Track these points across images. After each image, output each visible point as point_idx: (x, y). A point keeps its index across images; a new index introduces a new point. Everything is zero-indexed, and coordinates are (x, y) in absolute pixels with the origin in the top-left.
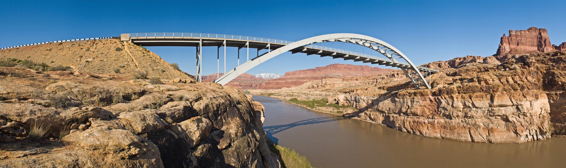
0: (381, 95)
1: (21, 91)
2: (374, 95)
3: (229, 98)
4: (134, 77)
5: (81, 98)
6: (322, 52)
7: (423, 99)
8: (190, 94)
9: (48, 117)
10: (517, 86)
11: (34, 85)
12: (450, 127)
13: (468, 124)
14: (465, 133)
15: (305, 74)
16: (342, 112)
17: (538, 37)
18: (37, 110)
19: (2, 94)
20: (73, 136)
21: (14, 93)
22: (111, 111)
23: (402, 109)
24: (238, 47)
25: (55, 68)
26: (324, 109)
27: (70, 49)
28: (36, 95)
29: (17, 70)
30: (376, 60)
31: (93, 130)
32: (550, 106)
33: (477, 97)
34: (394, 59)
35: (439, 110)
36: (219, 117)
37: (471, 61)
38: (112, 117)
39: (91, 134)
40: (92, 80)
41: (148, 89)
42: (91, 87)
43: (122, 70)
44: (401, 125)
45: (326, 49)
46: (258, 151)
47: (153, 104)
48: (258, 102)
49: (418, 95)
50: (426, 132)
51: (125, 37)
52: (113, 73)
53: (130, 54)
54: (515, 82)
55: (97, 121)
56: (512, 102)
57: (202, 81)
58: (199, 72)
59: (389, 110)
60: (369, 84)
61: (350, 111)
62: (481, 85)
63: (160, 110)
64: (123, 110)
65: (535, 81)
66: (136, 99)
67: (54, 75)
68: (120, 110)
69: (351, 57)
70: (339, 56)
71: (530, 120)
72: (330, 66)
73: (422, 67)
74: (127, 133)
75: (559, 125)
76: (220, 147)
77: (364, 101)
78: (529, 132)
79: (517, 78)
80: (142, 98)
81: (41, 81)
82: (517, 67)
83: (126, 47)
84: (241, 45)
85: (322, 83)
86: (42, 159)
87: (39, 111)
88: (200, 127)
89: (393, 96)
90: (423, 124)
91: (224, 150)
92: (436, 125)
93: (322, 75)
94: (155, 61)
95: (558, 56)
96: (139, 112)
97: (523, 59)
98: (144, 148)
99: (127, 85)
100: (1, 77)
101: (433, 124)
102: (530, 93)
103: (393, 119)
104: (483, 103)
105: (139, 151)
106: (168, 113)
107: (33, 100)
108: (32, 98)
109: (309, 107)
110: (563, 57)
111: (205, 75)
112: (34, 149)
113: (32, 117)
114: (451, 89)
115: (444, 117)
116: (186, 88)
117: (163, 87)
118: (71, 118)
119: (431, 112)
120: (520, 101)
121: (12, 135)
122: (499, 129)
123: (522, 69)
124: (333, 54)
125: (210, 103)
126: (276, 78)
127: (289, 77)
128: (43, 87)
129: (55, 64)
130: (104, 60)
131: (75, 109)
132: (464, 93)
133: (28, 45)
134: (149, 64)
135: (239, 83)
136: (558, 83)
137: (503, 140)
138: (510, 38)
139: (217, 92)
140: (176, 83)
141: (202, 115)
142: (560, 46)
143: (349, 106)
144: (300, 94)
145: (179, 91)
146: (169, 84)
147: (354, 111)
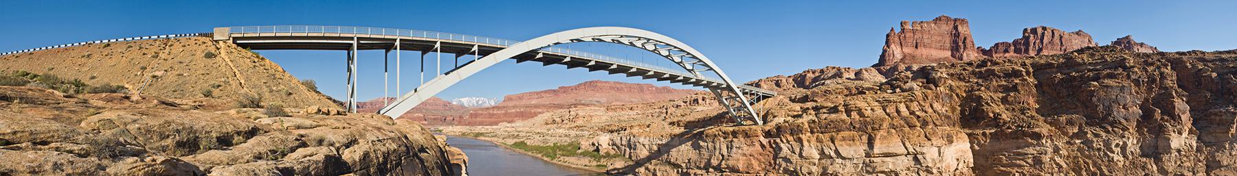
1: (38, 129)
10: (915, 120)
16: (606, 166)
17: (951, 34)
18: (65, 163)
19: (4, 134)
22: (197, 164)
23: (712, 161)
25: (97, 88)
29: (30, 92)
33: (844, 139)
35: (778, 162)
37: (834, 77)
42: (162, 121)
43: (216, 92)
45: (577, 55)
47: (270, 151)
48: (457, 149)
51: (221, 34)
52: (200, 97)
53: (230, 63)
54: (912, 113)
56: (906, 148)
59: (689, 162)
64: (218, 162)
65: (947, 111)
66: (241, 143)
67: (95, 101)
68: (213, 163)
69: (622, 69)
70: (599, 66)
73: (746, 87)
79: (915, 106)
80: (252, 141)
81: (73, 111)
82: (915, 86)
83: (222, 51)
84: (426, 47)
89: (695, 138)
95: (986, 66)
96: (246, 166)
99: (224, 118)
104: (855, 150)
107: (58, 144)
108: (57, 142)
109: (547, 157)
110: (996, 68)
114: (799, 126)
119: (763, 166)
125: (372, 150)
127: (510, 104)
130: (185, 74)
132: (822, 133)
133: (50, 48)
136: (988, 114)
139: (384, 130)
141: (357, 171)
142: (991, 50)
143: (618, 156)
144: (531, 134)
146: (299, 116)
147: (626, 165)
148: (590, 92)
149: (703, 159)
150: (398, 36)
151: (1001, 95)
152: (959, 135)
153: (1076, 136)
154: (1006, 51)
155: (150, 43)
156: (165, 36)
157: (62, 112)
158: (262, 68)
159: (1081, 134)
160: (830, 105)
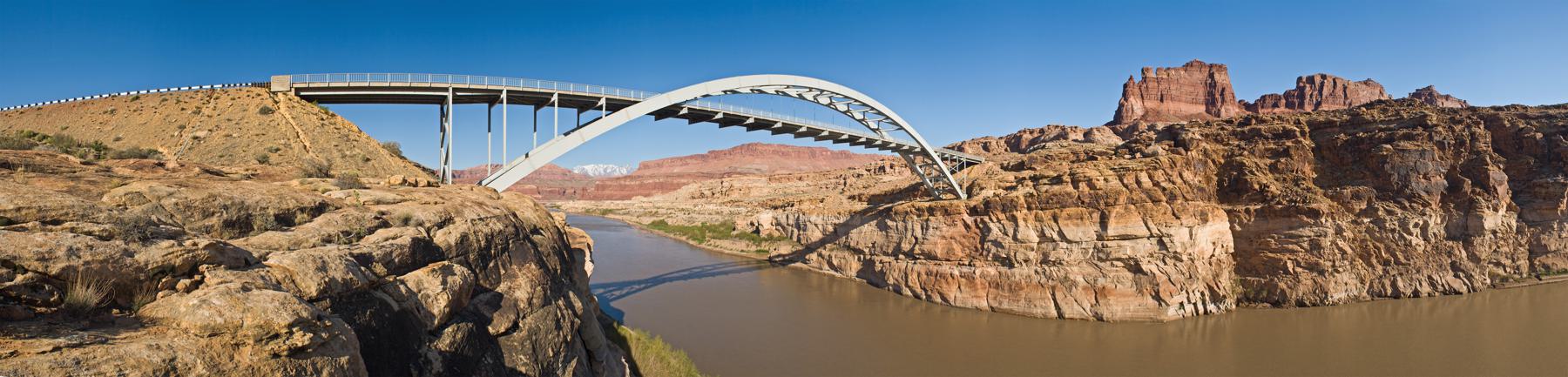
1: (48, 204)
2: (839, 214)
7: (949, 221)
9: (108, 263)
10: (1160, 193)
12: (1010, 286)
13: (1050, 278)
16: (767, 252)
18: (83, 248)
19: (5, 211)
20: (162, 306)
22: (250, 249)
23: (903, 245)
24: (533, 107)
25: (123, 152)
26: (727, 246)
29: (38, 158)
33: (1070, 217)
34: (884, 133)
35: (986, 247)
36: (490, 262)
37: (1057, 138)
38: (252, 263)
39: (205, 301)
41: (332, 200)
42: (205, 195)
43: (274, 158)
44: (900, 280)
45: (731, 110)
46: (578, 340)
47: (342, 232)
48: (580, 230)
49: (939, 213)
51: (280, 83)
52: (254, 164)
53: (291, 121)
54: (1156, 184)
56: (1148, 229)
57: (453, 183)
59: (874, 246)
61: (785, 249)
65: (1200, 182)
66: (306, 222)
67: (121, 169)
68: (269, 247)
70: (760, 125)
72: (741, 149)
73: (945, 151)
74: (285, 298)
76: (493, 329)
80: (319, 220)
81: (93, 181)
82: (1160, 150)
83: (282, 105)
84: (540, 101)
90: (950, 279)
91: (503, 338)
92: (978, 281)
96: (312, 252)
99: (285, 191)
101: (970, 279)
104: (1084, 231)
107: (74, 224)
109: (694, 239)
110: (1262, 127)
111: (460, 168)
113: (72, 264)
114: (1012, 200)
115: (997, 263)
119: (968, 251)
121: (25, 303)
123: (1172, 156)
124: (748, 122)
126: (621, 176)
127: (647, 173)
130: (234, 135)
132: (1042, 209)
133: (63, 101)
134: (334, 143)
136: (1252, 186)
139: (487, 206)
142: (1256, 104)
143: (784, 239)
144: (673, 211)
146: (379, 189)
147: (794, 250)
148: (748, 158)
150: (504, 86)
151: (1268, 161)
153: (1363, 213)
154: (1275, 105)
155: (191, 94)
158: (332, 127)
159: (1370, 211)
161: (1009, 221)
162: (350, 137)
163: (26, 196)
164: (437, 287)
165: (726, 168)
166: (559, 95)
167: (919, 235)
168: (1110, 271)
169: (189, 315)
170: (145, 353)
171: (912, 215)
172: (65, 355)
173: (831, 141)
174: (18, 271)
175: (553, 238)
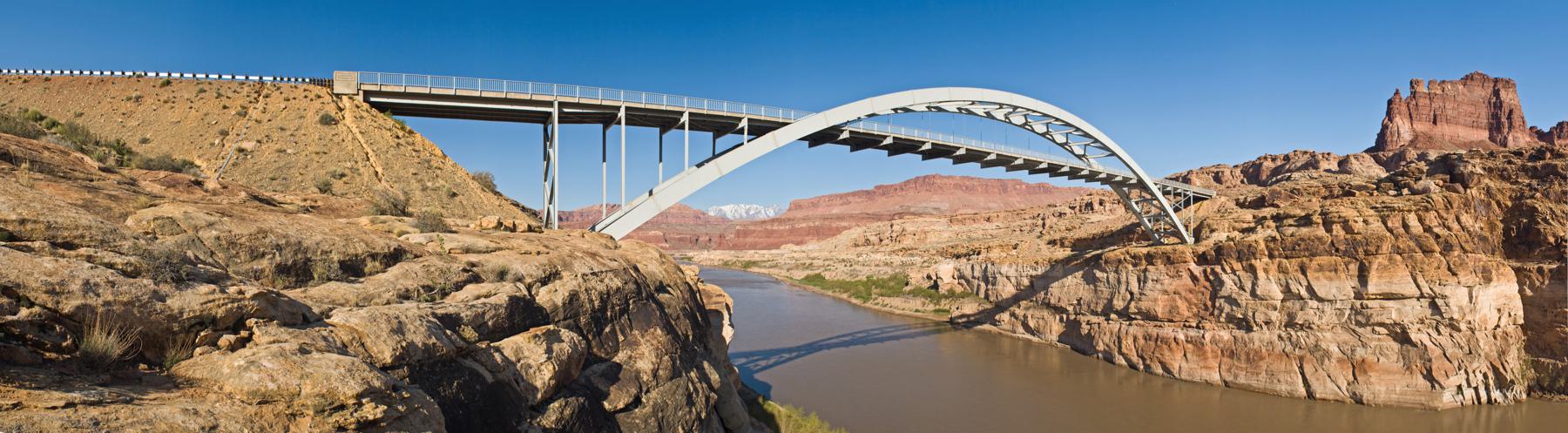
0: (1055, 261)
1: (60, 220)
2: (1037, 263)
3: (634, 275)
4: (372, 208)
5: (223, 262)
6: (892, 142)
7: (1172, 272)
8: (526, 263)
9: (134, 306)
10: (1432, 241)
11: (95, 206)
12: (1248, 354)
13: (1296, 345)
14: (1289, 372)
15: (846, 206)
16: (948, 311)
17: (1490, 103)
18: (102, 283)
19: (6, 221)
20: (200, 364)
21: (39, 222)
22: (309, 303)
23: (1115, 302)
24: (658, 129)
25: (151, 160)
26: (898, 304)
27: (193, 105)
28: (99, 238)
29: (46, 154)
30: (1041, 163)
31: (258, 353)
32: (1524, 305)
33: (1321, 268)
34: (1091, 160)
35: (1217, 304)
36: (606, 326)
37: (1305, 167)
38: (312, 320)
39: (253, 362)
40: (255, 210)
41: (410, 245)
42: (253, 229)
43: (338, 186)
44: (1112, 345)
45: (903, 133)
46: (714, 417)
47: (423, 287)
48: (716, 287)
49: (1159, 261)
50: (1180, 367)
51: (345, 82)
52: (313, 192)
53: (359, 136)
54: (1428, 229)
55: (270, 329)
56: (1418, 286)
57: (559, 227)
58: (551, 201)
59: (1079, 304)
60: (1021, 230)
61: (970, 308)
62: (1331, 235)
63: (443, 305)
64: (342, 301)
65: (1482, 229)
66: (378, 272)
67: (149, 184)
68: (333, 302)
69: (974, 156)
70: (939, 151)
71: (1469, 341)
72: (915, 183)
73: (1168, 183)
74: (353, 364)
75: (1548, 364)
76: (610, 404)
77: (1009, 280)
78: (1465, 376)
79: (1432, 218)
80: (395, 270)
81: (114, 196)
82: (1433, 187)
83: (347, 114)
84: (666, 122)
85: (892, 231)
86: (117, 419)
87: (109, 285)
88: (554, 354)
89: (1088, 265)
90: (1173, 345)
91: (623, 414)
92: (1208, 348)
93: (892, 209)
94: (429, 161)
95: (1545, 159)
96: (385, 309)
97: (1448, 163)
98: (399, 404)
99: (351, 231)
100: (3, 169)
101: (1198, 345)
102: (1467, 264)
103: (1090, 330)
104: (1338, 288)
105: (384, 412)
106: (467, 316)
107: (91, 251)
108: (89, 246)
109: (857, 297)
110: (1559, 163)
111: (567, 209)
112: (95, 389)
113: (89, 302)
114: (1250, 246)
115: (1231, 326)
116: (515, 245)
117: (452, 240)
118: (198, 313)
119: (1195, 310)
120: (1440, 284)
121: (31, 345)
122: (1384, 363)
123: (1447, 193)
124: (924, 148)
125: (583, 289)
126: (767, 219)
127: (799, 214)
128: (119, 217)
129: (153, 148)
130: (289, 151)
131: (207, 289)
132: (1287, 258)
133: (76, 72)
134: (413, 170)
135: (661, 234)
136: (1546, 239)
137: (1396, 396)
138: (1414, 102)
139: (602, 257)
140: (489, 231)
141: (559, 321)
142: (1551, 133)
143: (968, 295)
144: (831, 263)
145: (497, 253)
146: (468, 233)
147: (980, 309)
149: (1100, 298)
150: (622, 101)
152: (1502, 270)
155: (235, 86)
156: (257, 78)
157: (98, 196)
158: (410, 148)
160: (1300, 212)
161: (1247, 272)
162: (432, 163)
163: (31, 205)
164: (540, 355)
165: (897, 207)
166: (690, 114)
167: (1135, 289)
168: (1372, 340)
169: (234, 377)
170: (180, 418)
171: (1126, 264)
172: (80, 413)
173: (1027, 171)
174: (22, 302)
175: (683, 297)
